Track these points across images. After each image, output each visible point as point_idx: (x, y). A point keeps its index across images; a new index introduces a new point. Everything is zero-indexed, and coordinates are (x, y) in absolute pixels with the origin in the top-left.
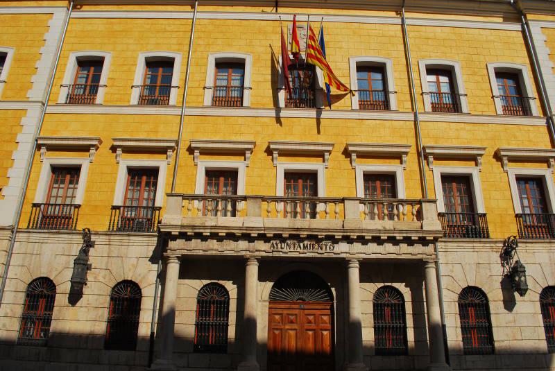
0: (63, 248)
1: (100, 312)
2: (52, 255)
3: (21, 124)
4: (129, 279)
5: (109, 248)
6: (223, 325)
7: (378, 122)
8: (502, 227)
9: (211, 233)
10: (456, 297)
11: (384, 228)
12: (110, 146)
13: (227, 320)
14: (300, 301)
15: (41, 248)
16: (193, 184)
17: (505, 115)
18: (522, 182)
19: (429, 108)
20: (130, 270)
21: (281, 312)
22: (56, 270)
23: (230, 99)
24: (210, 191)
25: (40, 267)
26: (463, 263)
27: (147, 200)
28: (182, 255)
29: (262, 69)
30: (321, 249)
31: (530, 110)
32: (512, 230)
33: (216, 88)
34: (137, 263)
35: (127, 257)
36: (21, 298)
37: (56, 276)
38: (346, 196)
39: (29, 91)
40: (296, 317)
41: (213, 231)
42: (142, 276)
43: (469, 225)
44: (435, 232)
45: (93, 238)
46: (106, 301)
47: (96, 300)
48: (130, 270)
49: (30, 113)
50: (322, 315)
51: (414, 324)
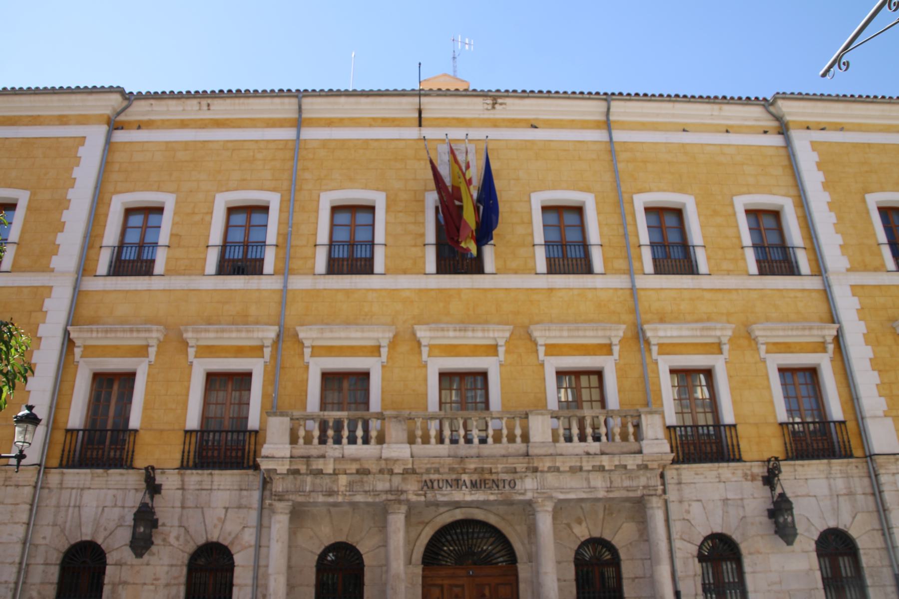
0: (114, 496)
1: (174, 591)
2: (97, 507)
3: (39, 335)
4: (215, 540)
5: (183, 494)
8: (760, 442)
15: (81, 496)
17: (762, 272)
18: (788, 374)
19: (649, 266)
20: (215, 526)
22: (105, 529)
23: (350, 259)
24: (494, 330)
25: (80, 526)
29: (401, 214)
30: (498, 486)
31: (798, 267)
32: (775, 447)
33: (332, 244)
34: (226, 515)
35: (209, 507)
36: (54, 573)
37: (105, 538)
39: (54, 258)
40: (442, 591)
42: (233, 535)
43: (706, 444)
45: (159, 479)
46: (182, 573)
47: (167, 573)
48: (215, 526)
49: (55, 293)
51: (105, 568)
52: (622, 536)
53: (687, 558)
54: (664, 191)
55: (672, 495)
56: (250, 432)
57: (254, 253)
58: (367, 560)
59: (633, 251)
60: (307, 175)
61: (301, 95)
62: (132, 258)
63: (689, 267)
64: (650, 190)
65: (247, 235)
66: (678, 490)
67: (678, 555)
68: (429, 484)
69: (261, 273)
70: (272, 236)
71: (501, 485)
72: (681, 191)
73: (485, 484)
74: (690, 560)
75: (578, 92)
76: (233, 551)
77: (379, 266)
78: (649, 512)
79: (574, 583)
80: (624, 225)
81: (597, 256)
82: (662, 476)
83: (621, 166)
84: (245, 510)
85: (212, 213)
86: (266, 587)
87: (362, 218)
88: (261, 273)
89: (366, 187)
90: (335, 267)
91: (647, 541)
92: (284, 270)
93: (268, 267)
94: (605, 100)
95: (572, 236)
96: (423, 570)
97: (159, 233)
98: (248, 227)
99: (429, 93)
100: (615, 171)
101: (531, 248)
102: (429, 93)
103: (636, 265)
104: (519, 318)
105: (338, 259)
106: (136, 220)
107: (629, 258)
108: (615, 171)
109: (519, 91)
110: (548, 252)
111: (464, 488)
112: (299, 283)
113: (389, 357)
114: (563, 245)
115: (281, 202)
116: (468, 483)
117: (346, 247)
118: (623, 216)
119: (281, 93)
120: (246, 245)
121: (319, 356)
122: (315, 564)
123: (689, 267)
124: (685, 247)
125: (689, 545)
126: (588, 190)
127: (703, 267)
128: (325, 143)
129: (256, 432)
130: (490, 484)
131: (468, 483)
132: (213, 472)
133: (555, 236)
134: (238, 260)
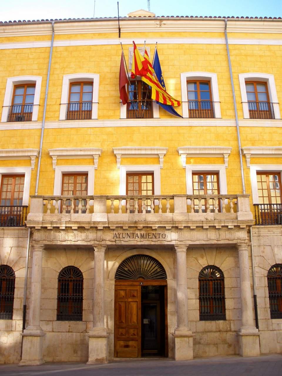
4: (5, 264)
6: (79, 299)
7: (205, 128)
9: (66, 227)
10: (266, 273)
11: (207, 219)
12: (256, 174)
13: (82, 295)
14: (141, 279)
16: (52, 185)
19: (247, 115)
21: (125, 288)
23: (79, 111)
26: (272, 246)
27: (268, 209)
28: (190, 245)
29: (107, 86)
30: (156, 237)
38: (175, 194)
41: (67, 225)
42: (15, 262)
44: (248, 221)
50: (120, 290)
52: (225, 263)
53: (261, 277)
54: (257, 72)
55: (254, 242)
56: (24, 207)
57: (27, 109)
58: (85, 276)
59: (238, 106)
60: (57, 66)
61: (53, 22)
62: (76, 110)
63: (269, 114)
64: (249, 71)
65: (24, 100)
66: (258, 240)
67: (256, 275)
68: (118, 236)
69: (90, 118)
70: (37, 100)
71: (157, 237)
72: (267, 72)
73: (149, 236)
74: (263, 278)
75: (213, 16)
76: (15, 269)
77: (94, 115)
78: (240, 252)
79: (198, 290)
80: (233, 91)
81: (217, 108)
82: (249, 232)
83: (232, 58)
84: (21, 248)
85: (5, 89)
86: (30, 288)
87: (86, 88)
88: (90, 118)
89: (89, 71)
90: (71, 115)
91: (239, 267)
92: (42, 119)
93: (34, 117)
94: (224, 21)
95: (262, 98)
96: (116, 281)
97: (34, 97)
98: (25, 95)
99: (124, 20)
100: (229, 61)
101: (241, 104)
102: (124, 20)
103: (239, 113)
104: (173, 146)
105: (72, 111)
106: (20, 91)
107: (234, 109)
108: (229, 61)
109: (175, 16)
110: (189, 106)
111: (137, 238)
112: (51, 125)
113: (100, 165)
114: (257, 102)
115: (42, 81)
116: (139, 235)
117: (194, 103)
118: (232, 86)
119: (43, 22)
120: (23, 106)
121: (61, 164)
122: (57, 277)
123: (269, 114)
124: (210, 103)
125: (263, 270)
126: (213, 71)
127: (277, 115)
128: (66, 48)
129: (27, 207)
130: (151, 236)
131: (139, 235)
132: (4, 228)
133: (252, 98)
134: (18, 114)
